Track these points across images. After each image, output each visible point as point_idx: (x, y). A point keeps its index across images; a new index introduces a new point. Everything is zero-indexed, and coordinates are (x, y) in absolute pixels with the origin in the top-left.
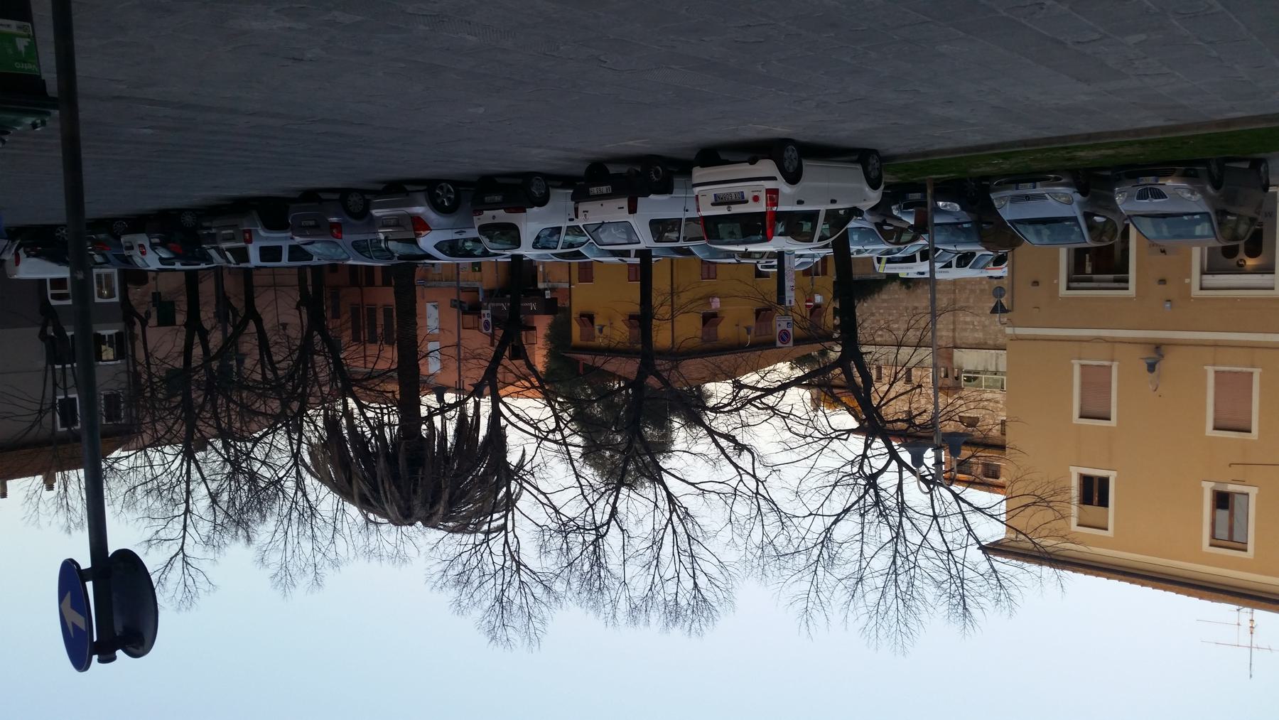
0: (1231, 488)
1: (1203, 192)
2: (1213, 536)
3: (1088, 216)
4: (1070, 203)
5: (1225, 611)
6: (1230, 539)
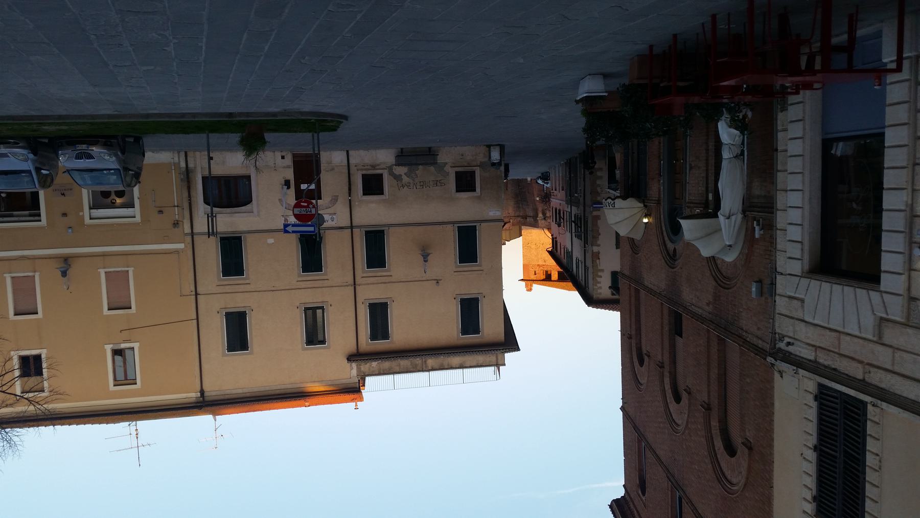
0: (123, 346)
1: (116, 155)
2: (115, 379)
3: (38, 170)
4: (26, 160)
5: (121, 428)
6: (125, 379)
